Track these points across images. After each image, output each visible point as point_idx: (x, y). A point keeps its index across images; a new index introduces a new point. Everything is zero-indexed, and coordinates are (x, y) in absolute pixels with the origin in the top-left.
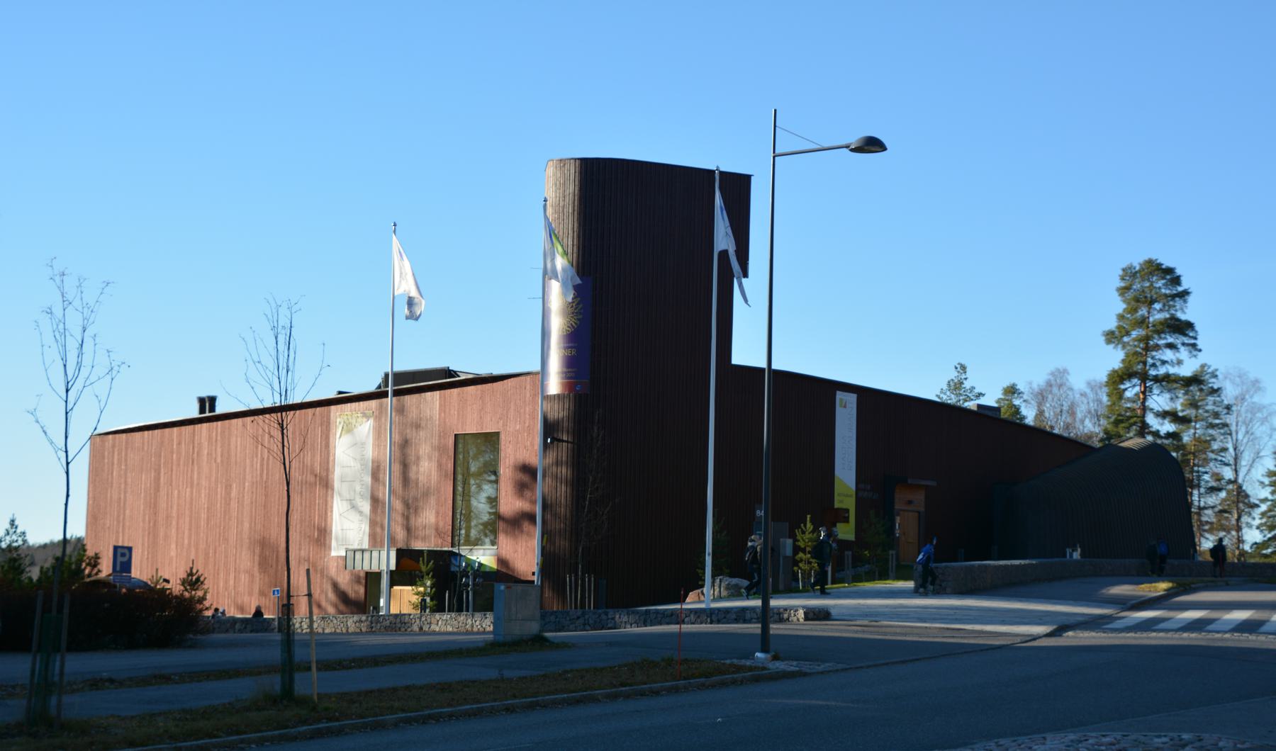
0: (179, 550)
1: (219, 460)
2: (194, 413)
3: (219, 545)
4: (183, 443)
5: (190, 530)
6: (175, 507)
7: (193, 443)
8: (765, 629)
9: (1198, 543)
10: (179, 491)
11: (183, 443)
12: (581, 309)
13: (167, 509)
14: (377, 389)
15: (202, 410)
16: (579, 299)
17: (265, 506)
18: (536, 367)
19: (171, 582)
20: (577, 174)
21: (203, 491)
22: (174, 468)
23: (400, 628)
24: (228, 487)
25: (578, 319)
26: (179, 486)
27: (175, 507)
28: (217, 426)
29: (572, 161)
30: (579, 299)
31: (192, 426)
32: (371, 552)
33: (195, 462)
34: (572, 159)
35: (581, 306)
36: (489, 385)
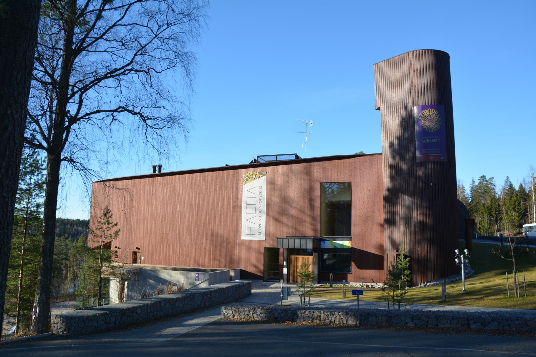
0: (145, 235)
1: (169, 193)
2: (151, 172)
3: (170, 233)
4: (147, 185)
5: (151, 225)
6: (142, 215)
7: (153, 185)
8: (358, 307)
9: (332, 305)
10: (145, 208)
11: (147, 185)
12: (440, 120)
13: (137, 215)
14: (250, 163)
15: (154, 171)
16: (439, 115)
17: (197, 215)
18: (275, 156)
19: (140, 249)
20: (433, 57)
21: (159, 208)
22: (142, 197)
23: (81, 292)
24: (174, 207)
25: (425, 128)
26: (144, 205)
27: (142, 215)
28: (167, 178)
29: (430, 51)
30: (439, 115)
31: (152, 178)
32: (307, 239)
33: (154, 194)
34: (427, 50)
35: (440, 119)
36: (342, 160)
